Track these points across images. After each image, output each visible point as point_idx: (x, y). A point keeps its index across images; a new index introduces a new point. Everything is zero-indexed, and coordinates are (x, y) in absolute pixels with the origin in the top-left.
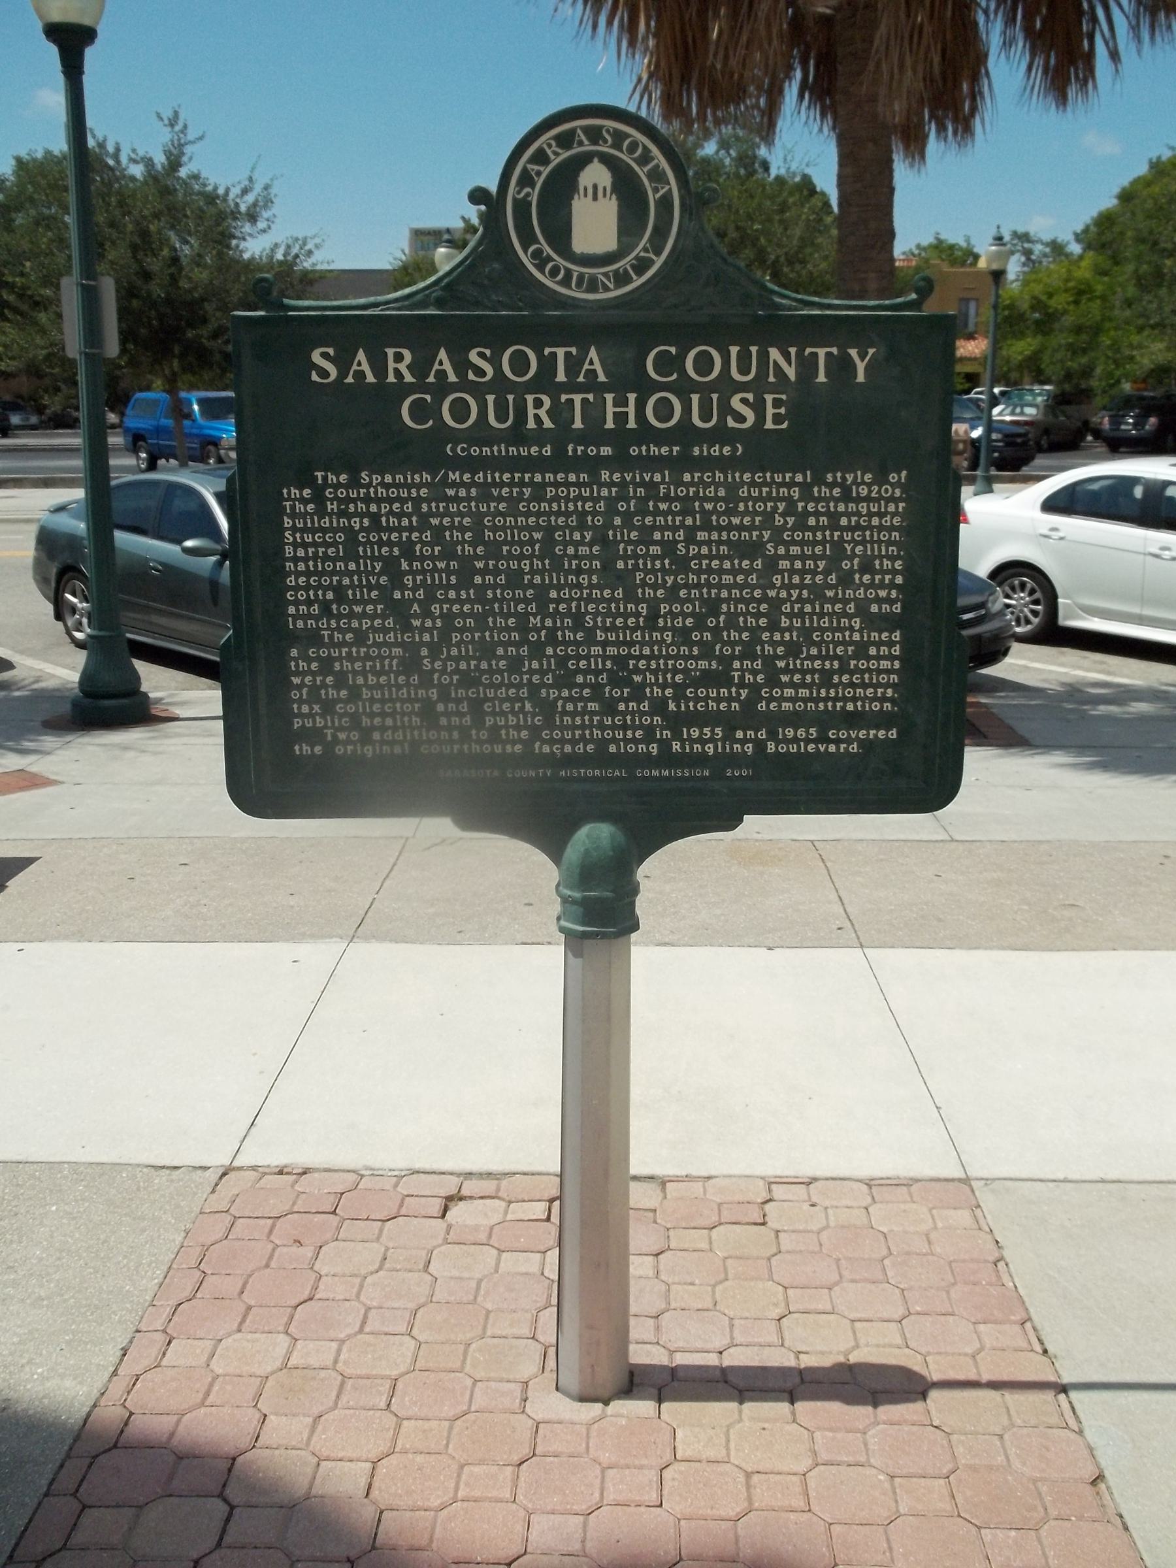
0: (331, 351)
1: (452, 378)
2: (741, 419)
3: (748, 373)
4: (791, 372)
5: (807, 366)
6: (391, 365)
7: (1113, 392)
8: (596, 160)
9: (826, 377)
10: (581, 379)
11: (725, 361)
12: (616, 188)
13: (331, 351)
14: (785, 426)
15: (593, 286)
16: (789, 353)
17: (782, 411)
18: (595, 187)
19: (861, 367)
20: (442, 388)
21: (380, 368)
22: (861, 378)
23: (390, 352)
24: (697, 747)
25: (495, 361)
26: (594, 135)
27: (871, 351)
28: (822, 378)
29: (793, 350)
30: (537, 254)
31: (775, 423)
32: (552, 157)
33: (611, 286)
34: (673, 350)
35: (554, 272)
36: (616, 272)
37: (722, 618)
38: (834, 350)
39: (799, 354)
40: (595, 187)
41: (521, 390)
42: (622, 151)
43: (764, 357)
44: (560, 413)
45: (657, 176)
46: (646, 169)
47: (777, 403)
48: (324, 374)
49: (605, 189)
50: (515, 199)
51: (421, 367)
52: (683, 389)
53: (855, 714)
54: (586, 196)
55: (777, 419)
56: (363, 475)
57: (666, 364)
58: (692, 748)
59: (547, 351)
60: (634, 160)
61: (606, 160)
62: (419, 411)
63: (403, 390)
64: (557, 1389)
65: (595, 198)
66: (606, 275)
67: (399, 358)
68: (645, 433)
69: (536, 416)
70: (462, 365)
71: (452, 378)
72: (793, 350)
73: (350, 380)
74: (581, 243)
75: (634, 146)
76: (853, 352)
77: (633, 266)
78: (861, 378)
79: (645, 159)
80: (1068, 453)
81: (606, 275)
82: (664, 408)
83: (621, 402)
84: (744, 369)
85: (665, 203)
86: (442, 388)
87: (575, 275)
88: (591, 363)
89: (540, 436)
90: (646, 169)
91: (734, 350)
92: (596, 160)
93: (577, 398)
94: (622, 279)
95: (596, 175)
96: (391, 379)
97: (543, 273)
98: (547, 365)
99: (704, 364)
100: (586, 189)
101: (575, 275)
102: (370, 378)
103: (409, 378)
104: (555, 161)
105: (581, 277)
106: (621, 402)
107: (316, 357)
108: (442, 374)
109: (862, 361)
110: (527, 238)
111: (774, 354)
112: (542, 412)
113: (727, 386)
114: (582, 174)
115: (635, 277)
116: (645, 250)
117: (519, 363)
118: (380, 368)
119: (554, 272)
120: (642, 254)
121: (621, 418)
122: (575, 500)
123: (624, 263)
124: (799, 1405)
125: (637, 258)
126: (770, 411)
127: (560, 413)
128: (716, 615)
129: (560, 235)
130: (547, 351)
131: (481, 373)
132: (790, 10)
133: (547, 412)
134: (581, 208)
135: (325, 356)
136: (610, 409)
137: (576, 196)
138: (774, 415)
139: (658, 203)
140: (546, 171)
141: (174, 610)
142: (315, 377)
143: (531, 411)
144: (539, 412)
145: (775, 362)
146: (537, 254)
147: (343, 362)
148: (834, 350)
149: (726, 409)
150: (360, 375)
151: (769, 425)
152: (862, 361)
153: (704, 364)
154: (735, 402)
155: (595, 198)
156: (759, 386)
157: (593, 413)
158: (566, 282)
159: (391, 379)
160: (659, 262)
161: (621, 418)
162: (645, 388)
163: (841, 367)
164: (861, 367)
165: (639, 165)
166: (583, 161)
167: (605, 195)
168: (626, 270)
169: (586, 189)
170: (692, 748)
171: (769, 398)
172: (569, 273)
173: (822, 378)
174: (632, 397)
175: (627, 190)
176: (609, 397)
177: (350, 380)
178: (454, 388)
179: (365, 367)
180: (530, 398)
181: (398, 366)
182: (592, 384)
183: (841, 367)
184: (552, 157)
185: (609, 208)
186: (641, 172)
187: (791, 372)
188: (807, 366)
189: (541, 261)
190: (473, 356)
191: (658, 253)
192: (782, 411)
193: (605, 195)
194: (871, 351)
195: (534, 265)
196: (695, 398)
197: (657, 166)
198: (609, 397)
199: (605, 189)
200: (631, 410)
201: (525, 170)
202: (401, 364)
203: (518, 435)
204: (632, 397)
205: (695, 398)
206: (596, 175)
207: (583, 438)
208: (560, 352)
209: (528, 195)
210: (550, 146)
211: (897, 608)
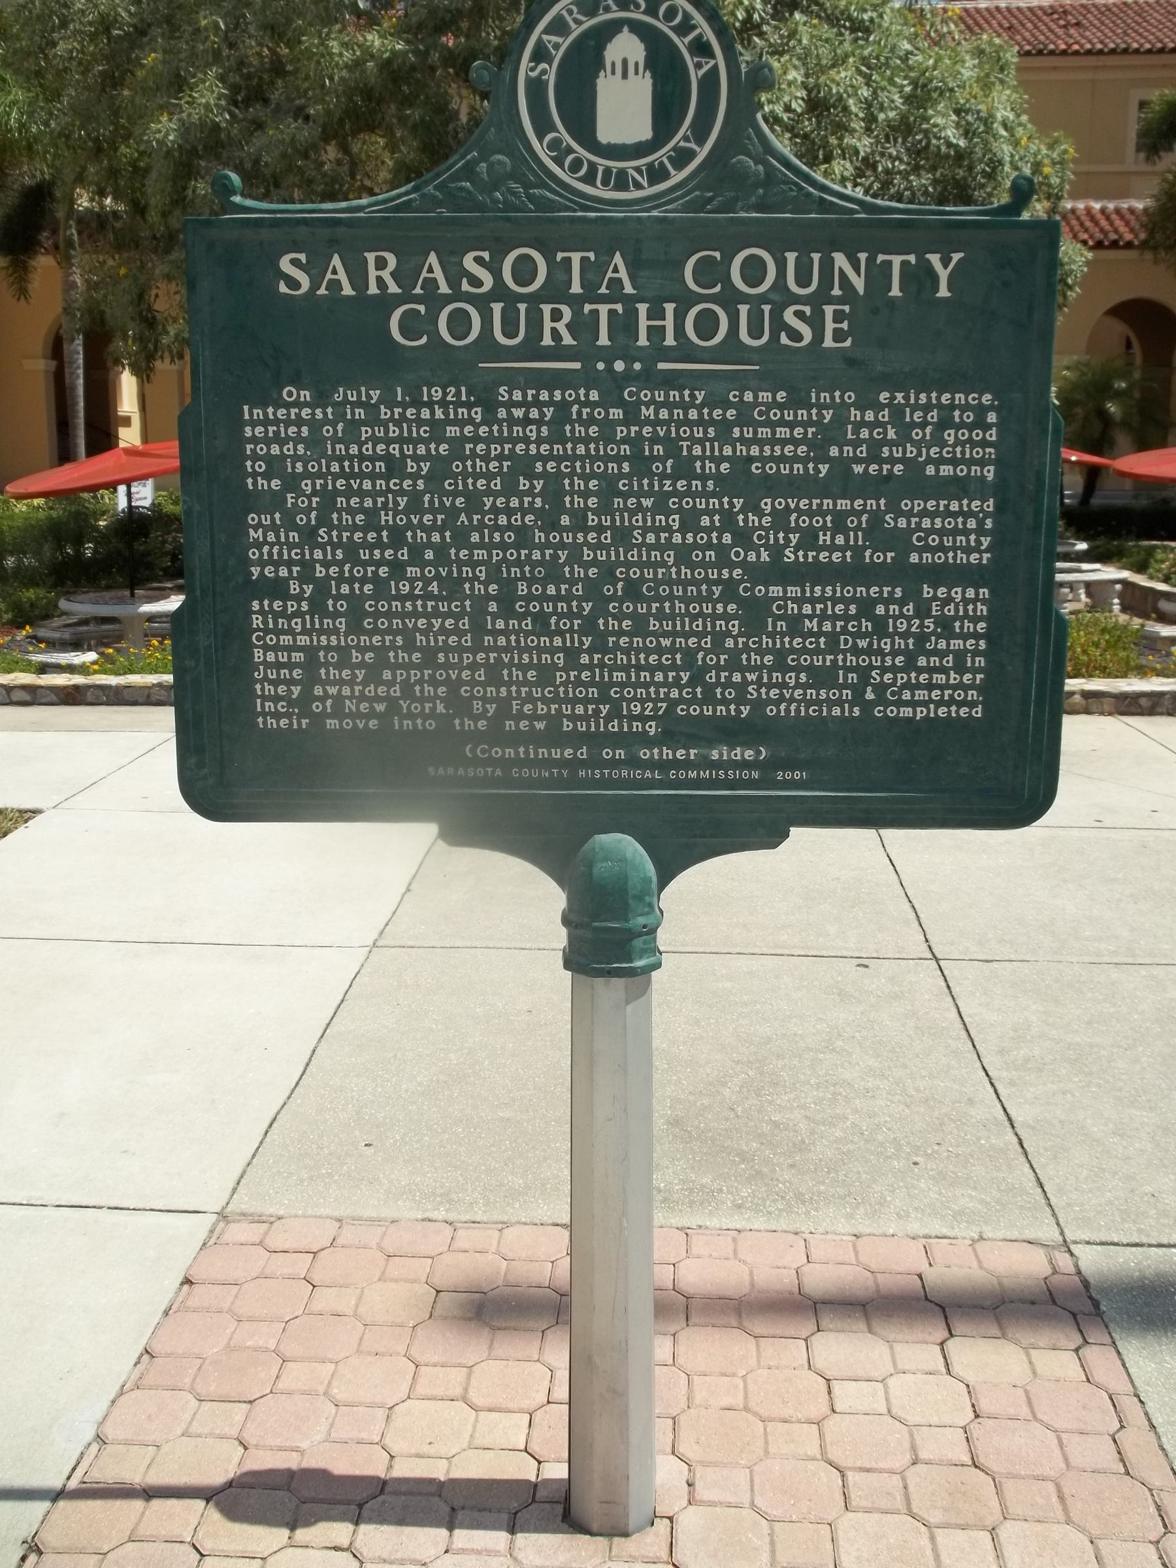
0: (302, 257)
1: (444, 289)
2: (796, 336)
3: (808, 285)
4: (859, 283)
5: (878, 276)
6: (373, 273)
7: (119, 333)
8: (626, 29)
9: (949, 290)
10: (418, 290)
12: (651, 63)
13: (302, 257)
14: (848, 343)
15: (622, 182)
16: (858, 260)
17: (845, 326)
18: (625, 62)
19: (943, 274)
20: (434, 300)
21: (358, 275)
23: (371, 257)
24: (637, 726)
27: (956, 257)
28: (895, 291)
29: (863, 256)
31: (835, 340)
32: (573, 25)
33: (645, 184)
34: (717, 255)
35: (576, 165)
36: (650, 166)
37: (620, 585)
38: (912, 258)
39: (871, 260)
40: (625, 62)
42: (657, 18)
43: (827, 266)
44: (583, 327)
45: (701, 48)
46: (687, 40)
47: (838, 317)
48: (294, 284)
49: (637, 64)
50: (528, 78)
54: (613, 73)
55: (838, 336)
56: (501, 390)
57: (709, 272)
58: (630, 727)
59: (560, 256)
60: (671, 28)
61: (638, 29)
63: (386, 303)
65: (625, 75)
66: (638, 170)
67: (381, 264)
69: (554, 331)
70: (455, 274)
71: (444, 289)
72: (863, 256)
73: (322, 291)
76: (935, 259)
77: (669, 158)
79: (685, 27)
80: (55, 428)
81: (638, 170)
82: (707, 325)
83: (656, 313)
85: (710, 82)
87: (601, 169)
88: (616, 270)
90: (687, 40)
92: (626, 29)
93: (603, 309)
95: (626, 48)
96: (373, 289)
97: (561, 166)
100: (613, 64)
101: (601, 169)
102: (348, 290)
103: (393, 288)
104: (577, 31)
105: (608, 171)
106: (656, 313)
107: (285, 264)
108: (431, 284)
109: (946, 267)
112: (561, 326)
113: (781, 297)
114: (609, 47)
115: (673, 172)
116: (686, 138)
118: (358, 275)
119: (576, 165)
120: (682, 144)
121: (656, 333)
122: (288, 439)
123: (661, 155)
124: (520, 1537)
125: (674, 149)
126: (830, 326)
127: (583, 327)
128: (614, 581)
129: (582, 119)
130: (560, 256)
131: (476, 282)
133: (567, 326)
134: (608, 88)
135: (295, 263)
136: (643, 323)
137: (602, 73)
138: (835, 330)
139: (702, 82)
142: (283, 288)
143: (548, 325)
145: (840, 269)
146: (555, 145)
147: (316, 267)
148: (912, 258)
149: (779, 325)
150: (335, 285)
151: (828, 342)
152: (946, 267)
154: (789, 316)
155: (625, 75)
158: (589, 179)
159: (373, 289)
160: (703, 153)
163: (920, 279)
164: (943, 274)
165: (679, 35)
166: (611, 30)
167: (637, 73)
168: (662, 163)
169: (613, 64)
170: (630, 727)
171: (829, 310)
172: (593, 167)
173: (895, 291)
174: (670, 308)
175: (664, 65)
176: (643, 308)
177: (322, 291)
178: (448, 299)
179: (342, 276)
180: (547, 309)
181: (380, 273)
184: (573, 25)
185: (642, 87)
186: (682, 44)
187: (859, 283)
188: (878, 276)
189: (560, 152)
190: (469, 262)
191: (701, 142)
192: (845, 326)
193: (637, 73)
194: (956, 257)
195: (552, 158)
196: (744, 309)
197: (700, 36)
198: (643, 308)
199: (637, 64)
200: (669, 323)
201: (540, 41)
204: (670, 308)
205: (744, 309)
206: (626, 48)
207: (609, 356)
209: (544, 72)
210: (570, 12)
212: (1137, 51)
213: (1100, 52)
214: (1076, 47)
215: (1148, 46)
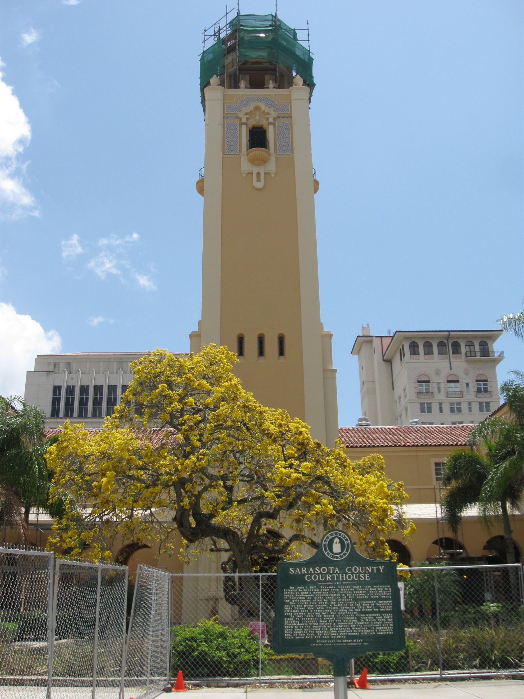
2: (362, 578)
5: (372, 570)
11: (359, 569)
21: (301, 571)
22: (382, 572)
25: (320, 570)
26: (336, 534)
28: (375, 572)
30: (328, 553)
41: (325, 574)
43: (365, 569)
44: (333, 578)
45: (346, 540)
48: (292, 572)
51: (307, 571)
52: (353, 573)
53: (386, 598)
55: (368, 578)
61: (338, 538)
62: (308, 578)
63: (305, 575)
64: (358, 337)
67: (304, 569)
68: (347, 581)
70: (314, 570)
74: (335, 551)
75: (342, 536)
76: (380, 567)
78: (382, 572)
79: (344, 537)
82: (349, 577)
84: (362, 571)
85: (348, 544)
86: (311, 574)
89: (329, 581)
91: (361, 568)
93: (335, 575)
94: (342, 557)
95: (337, 540)
98: (329, 570)
99: (355, 569)
103: (306, 573)
104: (330, 538)
107: (290, 569)
108: (311, 572)
110: (326, 550)
111: (367, 568)
117: (324, 570)
118: (301, 571)
121: (343, 578)
123: (342, 554)
126: (367, 577)
127: (333, 578)
129: (331, 549)
131: (317, 572)
132: (367, 644)
136: (341, 577)
140: (329, 540)
141: (248, 678)
144: (329, 577)
146: (328, 553)
147: (295, 570)
150: (297, 572)
153: (355, 569)
156: (365, 573)
157: (338, 577)
160: (348, 554)
161: (343, 578)
162: (346, 574)
163: (378, 570)
166: (335, 538)
182: (337, 573)
183: (378, 570)
185: (339, 545)
186: (344, 539)
188: (372, 570)
190: (316, 569)
200: (344, 577)
202: (304, 570)
203: (325, 581)
206: (337, 540)
208: (331, 568)
211: (393, 633)
212: (431, 445)
213: (417, 445)
214: (408, 444)
215: (434, 444)
